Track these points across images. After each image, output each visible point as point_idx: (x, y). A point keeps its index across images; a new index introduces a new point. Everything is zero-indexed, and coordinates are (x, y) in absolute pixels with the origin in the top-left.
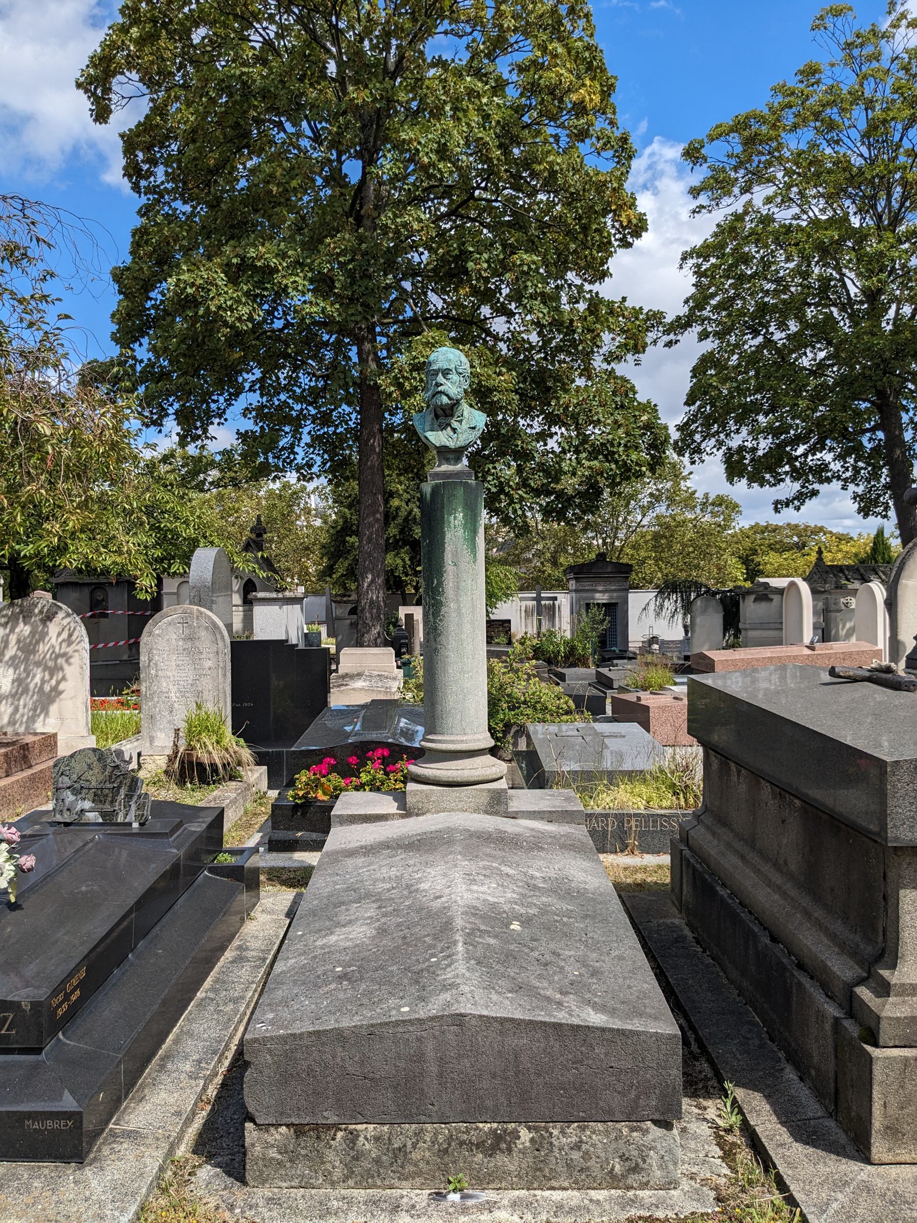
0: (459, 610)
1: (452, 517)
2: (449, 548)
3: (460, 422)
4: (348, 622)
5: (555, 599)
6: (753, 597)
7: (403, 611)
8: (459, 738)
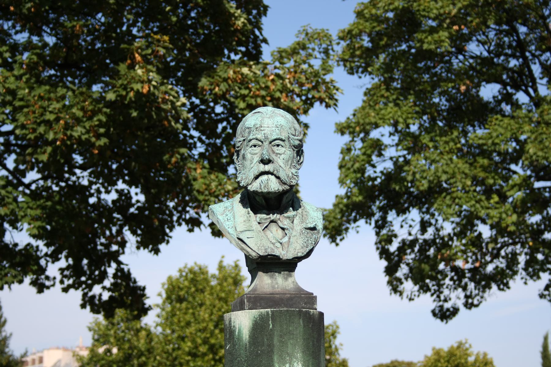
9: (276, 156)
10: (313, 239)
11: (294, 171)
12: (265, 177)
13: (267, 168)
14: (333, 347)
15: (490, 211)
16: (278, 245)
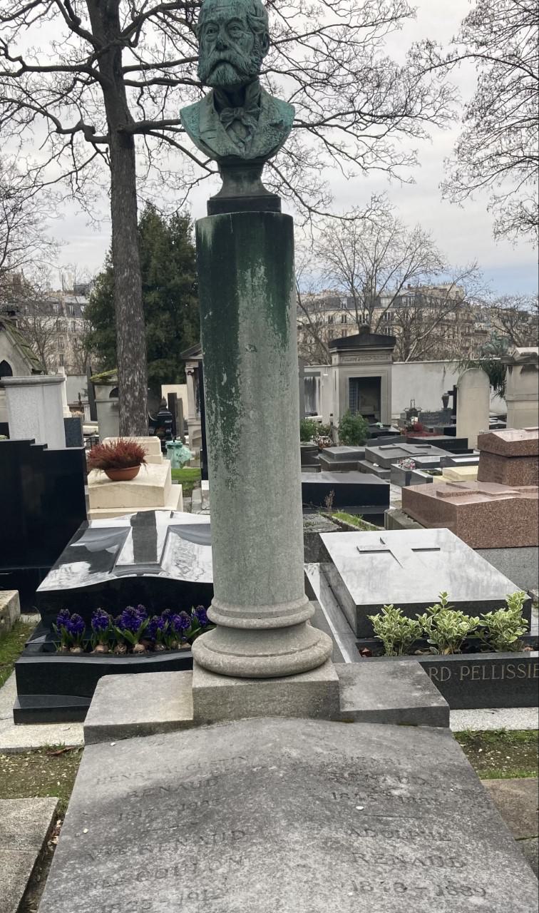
0: (261, 422)
1: (248, 273)
2: (244, 325)
3: (257, 116)
4: (110, 405)
5: (319, 374)
6: (519, 368)
7: (166, 390)
8: (266, 609)
9: (234, 41)
10: (278, 137)
11: (254, 58)
12: (221, 68)
13: (222, 55)
14: (436, 293)
15: (525, 842)
16: (241, 144)
